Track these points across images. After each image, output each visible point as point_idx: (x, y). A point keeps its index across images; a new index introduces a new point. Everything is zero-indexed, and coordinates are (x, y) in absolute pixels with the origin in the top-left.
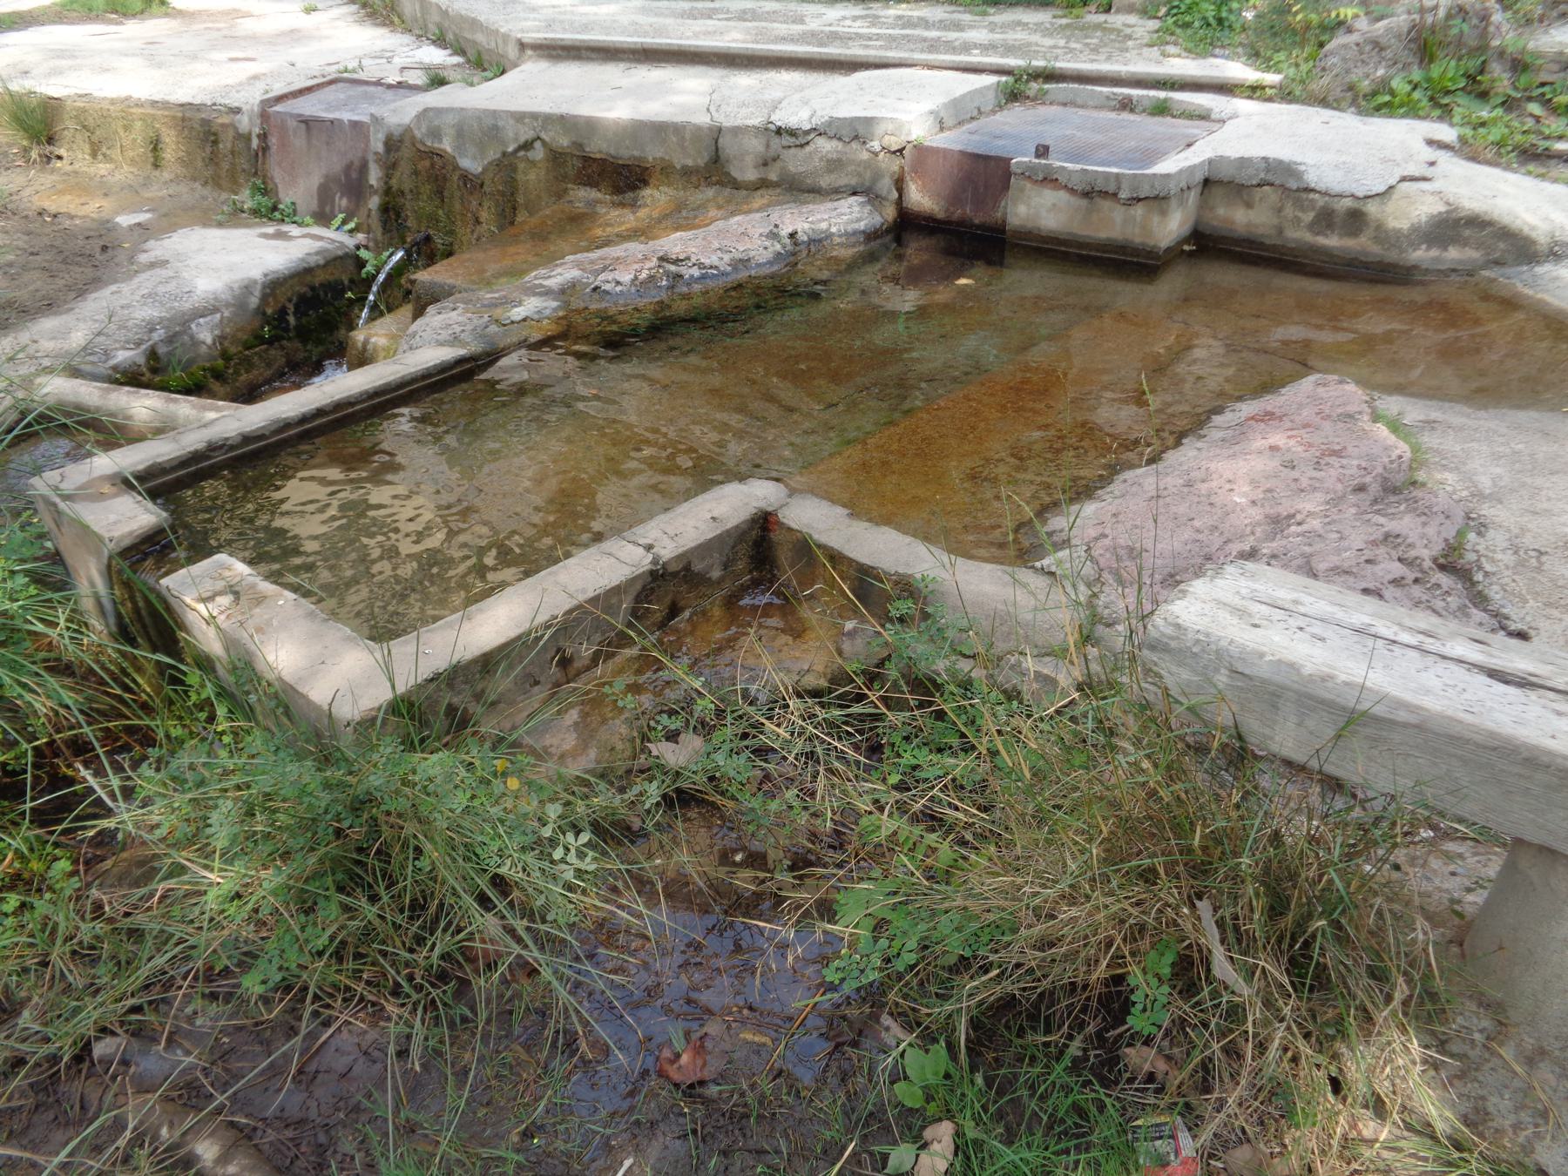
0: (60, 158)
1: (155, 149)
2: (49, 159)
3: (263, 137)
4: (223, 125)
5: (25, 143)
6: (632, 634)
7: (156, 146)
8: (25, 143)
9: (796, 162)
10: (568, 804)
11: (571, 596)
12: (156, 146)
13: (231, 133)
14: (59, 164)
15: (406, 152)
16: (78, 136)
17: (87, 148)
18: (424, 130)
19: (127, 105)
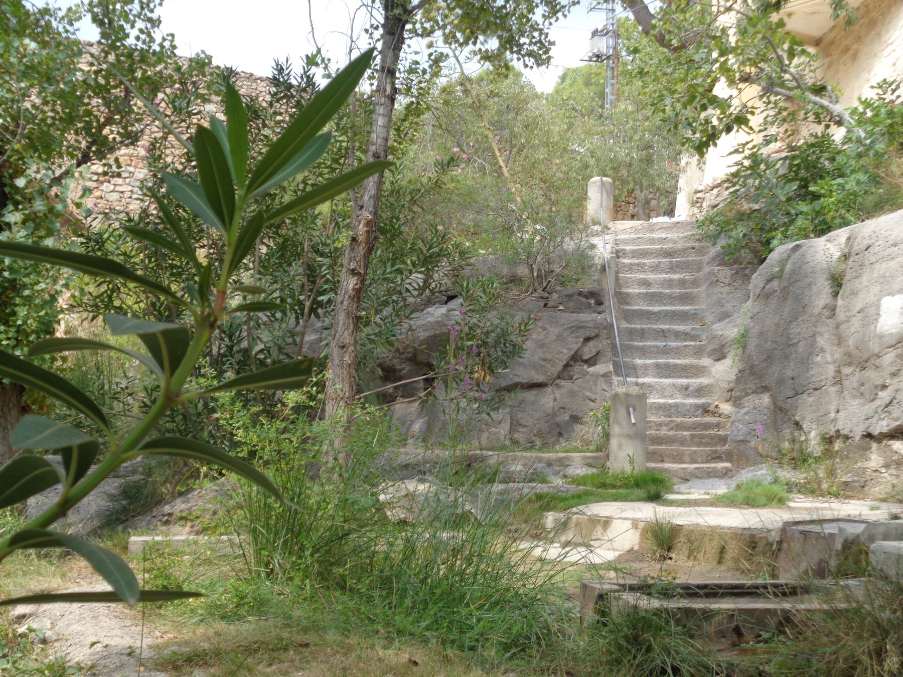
0: (671, 558)
1: (721, 552)
2: (665, 559)
3: (780, 543)
4: (761, 538)
5: (655, 548)
6: (676, 276)
7: (722, 550)
8: (655, 548)
9: (576, 500)
10: (194, 220)
11: (850, 280)
12: (722, 550)
13: (764, 541)
14: (669, 562)
15: (854, 548)
16: (684, 546)
17: (687, 553)
18: (866, 537)
19: (713, 529)
